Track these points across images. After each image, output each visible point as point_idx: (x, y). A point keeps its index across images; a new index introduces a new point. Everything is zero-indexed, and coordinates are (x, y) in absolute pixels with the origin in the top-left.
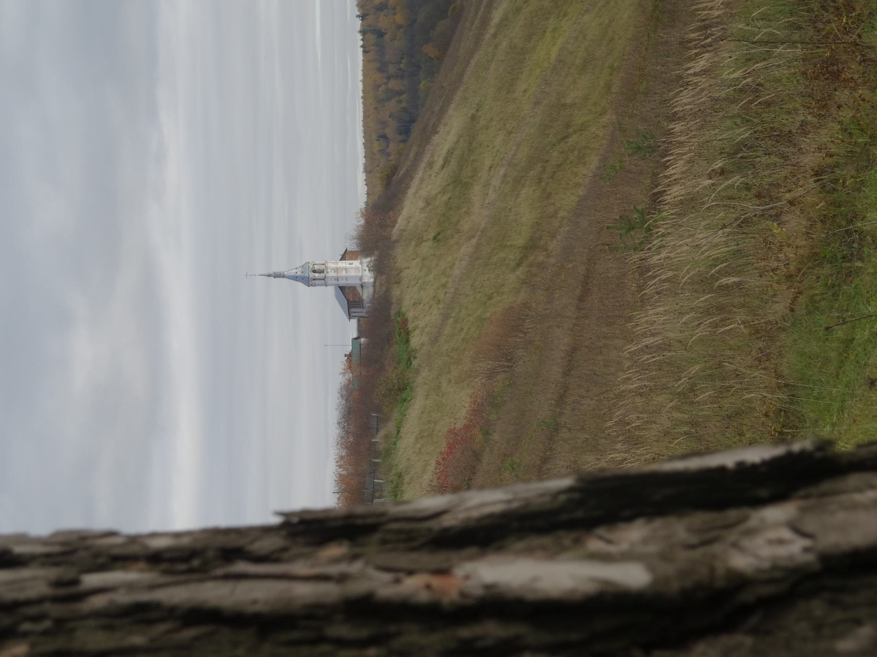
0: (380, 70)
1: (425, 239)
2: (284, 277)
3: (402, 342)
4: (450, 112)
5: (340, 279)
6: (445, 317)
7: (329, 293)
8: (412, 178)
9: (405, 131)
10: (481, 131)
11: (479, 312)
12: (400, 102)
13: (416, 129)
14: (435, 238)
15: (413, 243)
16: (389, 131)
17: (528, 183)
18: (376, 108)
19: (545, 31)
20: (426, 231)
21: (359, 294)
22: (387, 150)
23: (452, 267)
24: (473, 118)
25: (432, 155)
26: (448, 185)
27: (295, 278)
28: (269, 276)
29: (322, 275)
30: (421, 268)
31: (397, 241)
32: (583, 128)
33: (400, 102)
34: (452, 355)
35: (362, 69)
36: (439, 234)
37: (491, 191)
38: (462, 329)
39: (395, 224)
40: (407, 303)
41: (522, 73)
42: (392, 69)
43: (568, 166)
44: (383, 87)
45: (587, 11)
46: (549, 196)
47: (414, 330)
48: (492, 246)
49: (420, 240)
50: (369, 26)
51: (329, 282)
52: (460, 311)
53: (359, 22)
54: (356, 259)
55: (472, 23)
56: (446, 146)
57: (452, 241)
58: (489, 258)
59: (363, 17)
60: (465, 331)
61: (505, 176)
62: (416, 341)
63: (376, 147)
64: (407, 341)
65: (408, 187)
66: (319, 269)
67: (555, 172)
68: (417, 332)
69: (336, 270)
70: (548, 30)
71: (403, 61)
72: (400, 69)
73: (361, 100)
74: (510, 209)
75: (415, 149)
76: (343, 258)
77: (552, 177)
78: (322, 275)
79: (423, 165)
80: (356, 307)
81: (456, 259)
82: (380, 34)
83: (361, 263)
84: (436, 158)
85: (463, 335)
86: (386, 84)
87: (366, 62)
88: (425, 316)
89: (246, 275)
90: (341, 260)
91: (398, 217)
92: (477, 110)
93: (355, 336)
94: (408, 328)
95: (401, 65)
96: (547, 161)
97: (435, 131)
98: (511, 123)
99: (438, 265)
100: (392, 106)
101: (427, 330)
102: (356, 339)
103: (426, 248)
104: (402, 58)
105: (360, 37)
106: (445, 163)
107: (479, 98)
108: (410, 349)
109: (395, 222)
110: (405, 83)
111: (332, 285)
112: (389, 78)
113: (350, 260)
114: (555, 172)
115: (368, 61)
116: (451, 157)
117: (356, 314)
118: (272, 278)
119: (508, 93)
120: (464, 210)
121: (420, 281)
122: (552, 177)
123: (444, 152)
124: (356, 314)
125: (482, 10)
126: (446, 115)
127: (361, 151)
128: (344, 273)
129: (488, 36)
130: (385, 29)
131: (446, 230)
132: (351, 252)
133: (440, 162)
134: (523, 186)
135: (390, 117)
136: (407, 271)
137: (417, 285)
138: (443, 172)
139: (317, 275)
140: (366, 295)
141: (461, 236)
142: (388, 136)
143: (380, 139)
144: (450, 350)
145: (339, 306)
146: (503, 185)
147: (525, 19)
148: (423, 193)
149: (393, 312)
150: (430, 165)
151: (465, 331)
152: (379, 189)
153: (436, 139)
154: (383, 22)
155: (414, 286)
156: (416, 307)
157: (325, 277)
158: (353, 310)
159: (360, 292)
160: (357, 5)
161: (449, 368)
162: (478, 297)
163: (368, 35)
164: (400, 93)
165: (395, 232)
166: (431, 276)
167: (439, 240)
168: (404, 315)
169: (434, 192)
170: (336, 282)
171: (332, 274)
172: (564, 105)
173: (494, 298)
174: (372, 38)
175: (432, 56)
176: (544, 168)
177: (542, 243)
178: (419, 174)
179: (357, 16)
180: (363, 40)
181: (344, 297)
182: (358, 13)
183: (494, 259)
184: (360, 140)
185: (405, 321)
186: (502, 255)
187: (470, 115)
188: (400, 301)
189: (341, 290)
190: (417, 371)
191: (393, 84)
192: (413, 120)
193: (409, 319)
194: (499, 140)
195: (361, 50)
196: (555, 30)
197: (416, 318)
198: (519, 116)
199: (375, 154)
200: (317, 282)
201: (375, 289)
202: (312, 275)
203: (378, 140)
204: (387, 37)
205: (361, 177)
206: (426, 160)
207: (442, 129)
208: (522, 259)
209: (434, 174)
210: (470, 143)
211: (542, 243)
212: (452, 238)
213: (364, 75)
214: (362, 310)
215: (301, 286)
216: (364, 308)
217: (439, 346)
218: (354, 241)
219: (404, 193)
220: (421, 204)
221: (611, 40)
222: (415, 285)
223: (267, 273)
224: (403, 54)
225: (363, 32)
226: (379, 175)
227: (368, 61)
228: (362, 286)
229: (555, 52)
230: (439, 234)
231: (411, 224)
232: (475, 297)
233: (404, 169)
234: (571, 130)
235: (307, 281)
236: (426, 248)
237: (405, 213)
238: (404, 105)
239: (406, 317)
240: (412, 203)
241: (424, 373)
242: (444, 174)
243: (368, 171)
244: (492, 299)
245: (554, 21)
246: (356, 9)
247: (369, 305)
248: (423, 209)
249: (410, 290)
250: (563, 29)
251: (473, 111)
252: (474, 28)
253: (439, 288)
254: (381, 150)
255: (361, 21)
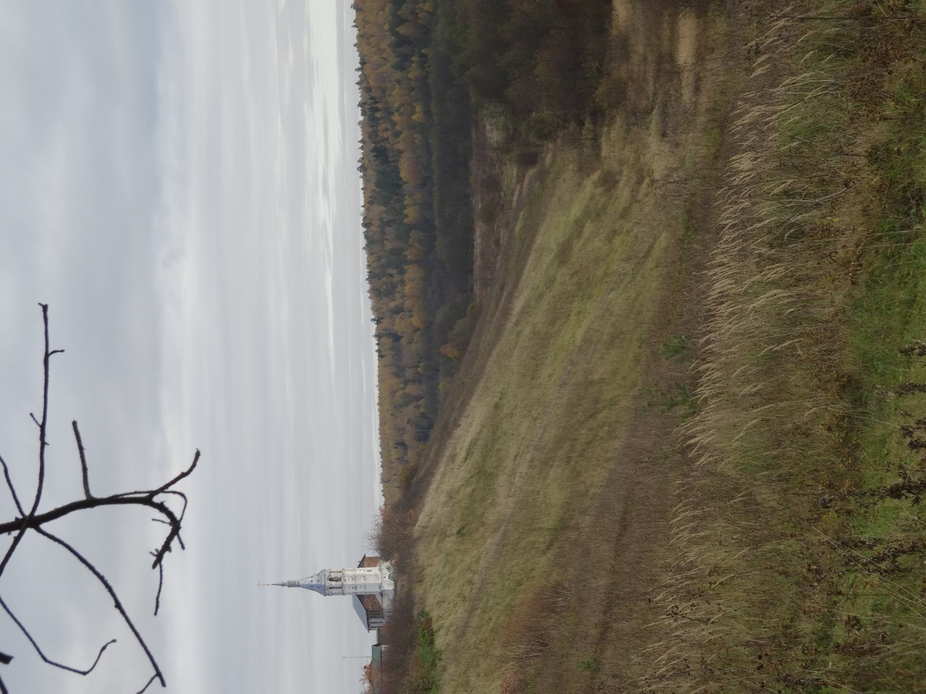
0: (397, 375)
1: (448, 534)
2: (299, 586)
3: (426, 643)
4: (473, 403)
5: (358, 587)
6: (471, 612)
7: (345, 604)
8: (433, 474)
9: (423, 437)
10: (505, 419)
11: (508, 600)
12: (418, 407)
13: (435, 433)
14: (459, 532)
15: (436, 539)
16: (407, 438)
17: (556, 463)
18: (393, 415)
19: (569, 315)
20: (449, 526)
21: (378, 603)
22: (405, 458)
23: (477, 562)
24: (497, 406)
25: (455, 449)
26: (472, 477)
27: (311, 587)
28: (283, 585)
29: (339, 584)
30: (445, 565)
31: (420, 538)
32: (613, 403)
33: (418, 407)
34: (481, 646)
35: (361, 133)
36: (463, 528)
37: (517, 479)
38: (490, 619)
39: (416, 522)
40: (431, 601)
41: (546, 358)
42: (409, 374)
43: (598, 443)
44: (400, 392)
45: (612, 290)
46: (579, 474)
47: (439, 630)
48: (521, 531)
49: (443, 535)
50: (385, 329)
51: (347, 590)
52: (488, 600)
53: (374, 326)
54: (375, 566)
55: (493, 317)
56: (469, 438)
57: (477, 535)
58: (517, 544)
59: (378, 321)
60: (493, 621)
61: (532, 461)
62: (440, 641)
63: (394, 454)
64: (432, 642)
65: (429, 484)
66: (336, 577)
67: (584, 450)
68: (442, 632)
69: (354, 578)
70: (572, 314)
71: (420, 365)
72: (418, 373)
73: (378, 407)
74: (538, 492)
75: (435, 447)
76: (361, 565)
77: (582, 455)
78: (339, 584)
79: (445, 459)
80: (375, 617)
81: (482, 553)
82: (396, 338)
83: (380, 570)
84: (458, 451)
85: (492, 624)
86: (404, 389)
87: (381, 367)
88: (450, 615)
89: (259, 585)
90: (358, 567)
91: (419, 515)
92: (501, 398)
93: (376, 643)
94: (432, 628)
95: (419, 369)
96: (576, 439)
97: (456, 425)
98: (536, 410)
99: (462, 561)
100: (410, 411)
101: (452, 629)
102: (376, 645)
103: (449, 544)
104: (420, 362)
105: (375, 341)
106: (468, 455)
107: (502, 386)
108: (434, 651)
109: (416, 520)
110: (423, 387)
111: (350, 593)
112: (406, 383)
113: (369, 566)
114: (584, 450)
115: (384, 366)
116: (474, 448)
117: (375, 625)
118: (286, 587)
119: (533, 379)
120: (489, 501)
121: (444, 578)
122: (582, 455)
123: (466, 444)
124: (375, 625)
125: (503, 301)
126: (467, 408)
127: (377, 460)
128: (362, 581)
129: (509, 325)
130: (401, 333)
131: (471, 524)
132: (370, 558)
133: (462, 454)
134: (552, 466)
135: (408, 423)
136: (430, 569)
137: (441, 583)
138: (466, 464)
139: (333, 583)
140: (386, 604)
141: (486, 529)
142: (406, 443)
143: (397, 446)
144: (478, 642)
145: (357, 614)
146: (530, 470)
147: (549, 303)
148: (446, 487)
149: (415, 612)
150: (453, 458)
151: (493, 621)
152: (398, 495)
153: (458, 432)
154: (399, 325)
155: (438, 584)
156: (441, 606)
157: (342, 585)
158: (373, 620)
159: (380, 601)
160: (372, 308)
161: (478, 661)
162: (507, 584)
163: (384, 339)
164: (418, 398)
165: (416, 530)
166: (456, 573)
167: (463, 535)
168: (427, 614)
169: (457, 485)
170: (354, 590)
171: (349, 582)
172: (592, 382)
173: (523, 584)
174: (387, 341)
175: (451, 356)
176: (573, 446)
177: (573, 522)
178: (441, 468)
179: (372, 320)
180: (378, 344)
181: (363, 607)
182: (373, 317)
183: (522, 544)
184: (376, 449)
185: (429, 621)
186: (531, 539)
187: (492, 404)
188: (423, 600)
189: (360, 599)
190: (444, 669)
191: (411, 389)
192: (430, 427)
193: (433, 619)
194: (523, 428)
195: (376, 355)
196: (579, 313)
197: (441, 617)
198: (545, 402)
199: (393, 463)
200: (334, 591)
201: (396, 594)
202: (329, 583)
203: (396, 448)
204: (403, 341)
205: (378, 487)
206: (447, 454)
207: (464, 422)
208: (552, 541)
209: (457, 467)
210: (494, 433)
211: (573, 522)
212: (477, 531)
213: (380, 381)
214: (383, 620)
215: (315, 595)
216: (383, 618)
217: (466, 639)
218: (373, 541)
219: (425, 491)
220: (443, 499)
221: (639, 313)
222: (439, 582)
223: (280, 582)
224: (421, 358)
225: (379, 336)
226: (396, 484)
227: (384, 366)
228: (382, 595)
229: (580, 334)
230: (463, 528)
231: (433, 520)
232: (504, 585)
233: (424, 469)
234: (600, 406)
235: (324, 590)
236: (449, 544)
237: (427, 509)
238: (422, 410)
239: (430, 616)
240: (434, 499)
241: (451, 669)
242: (467, 465)
243: (385, 481)
244: (521, 584)
245: (578, 303)
246: (371, 312)
247: (389, 614)
248: (445, 504)
249: (433, 588)
250: (588, 311)
251: (496, 400)
252: (494, 320)
253: (464, 585)
254: (399, 459)
255: (376, 325)
